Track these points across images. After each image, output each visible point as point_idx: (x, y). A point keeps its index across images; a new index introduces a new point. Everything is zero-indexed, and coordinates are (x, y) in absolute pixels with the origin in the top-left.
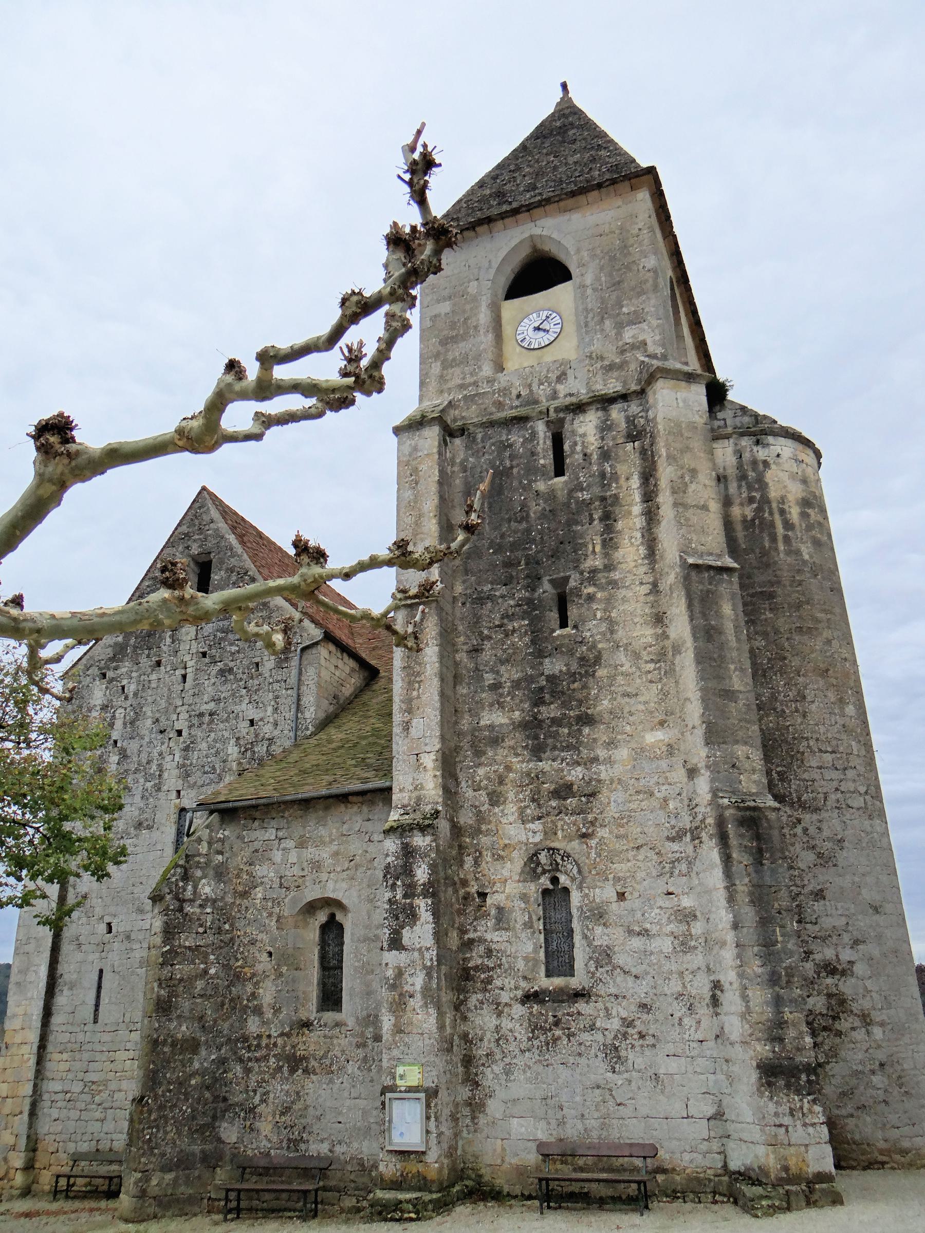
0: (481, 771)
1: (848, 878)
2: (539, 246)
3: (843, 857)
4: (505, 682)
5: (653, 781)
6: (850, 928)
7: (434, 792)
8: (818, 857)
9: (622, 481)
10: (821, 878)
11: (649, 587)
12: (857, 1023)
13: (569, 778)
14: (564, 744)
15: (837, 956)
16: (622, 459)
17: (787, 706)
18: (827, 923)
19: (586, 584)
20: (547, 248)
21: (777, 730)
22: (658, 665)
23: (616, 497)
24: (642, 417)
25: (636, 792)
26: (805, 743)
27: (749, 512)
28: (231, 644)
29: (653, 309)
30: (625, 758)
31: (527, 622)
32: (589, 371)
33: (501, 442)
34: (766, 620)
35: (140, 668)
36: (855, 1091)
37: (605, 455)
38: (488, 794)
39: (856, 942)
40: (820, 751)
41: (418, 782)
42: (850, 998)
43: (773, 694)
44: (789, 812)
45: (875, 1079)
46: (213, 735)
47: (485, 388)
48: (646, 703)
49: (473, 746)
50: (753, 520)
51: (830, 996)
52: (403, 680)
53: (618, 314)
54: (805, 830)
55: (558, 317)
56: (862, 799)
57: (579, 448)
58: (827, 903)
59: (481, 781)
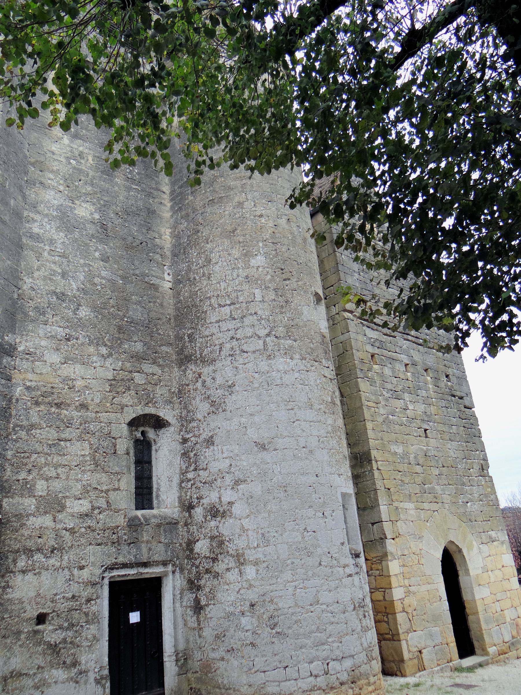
1: (236, 420)
3: (231, 401)
6: (233, 469)
8: (212, 406)
10: (213, 425)
12: (232, 564)
15: (220, 498)
18: (214, 467)
26: (208, 303)
36: (227, 634)
39: (237, 482)
40: (220, 306)
42: (227, 539)
44: (194, 370)
45: (244, 621)
51: (212, 538)
54: (204, 382)
56: (261, 342)
58: (216, 448)
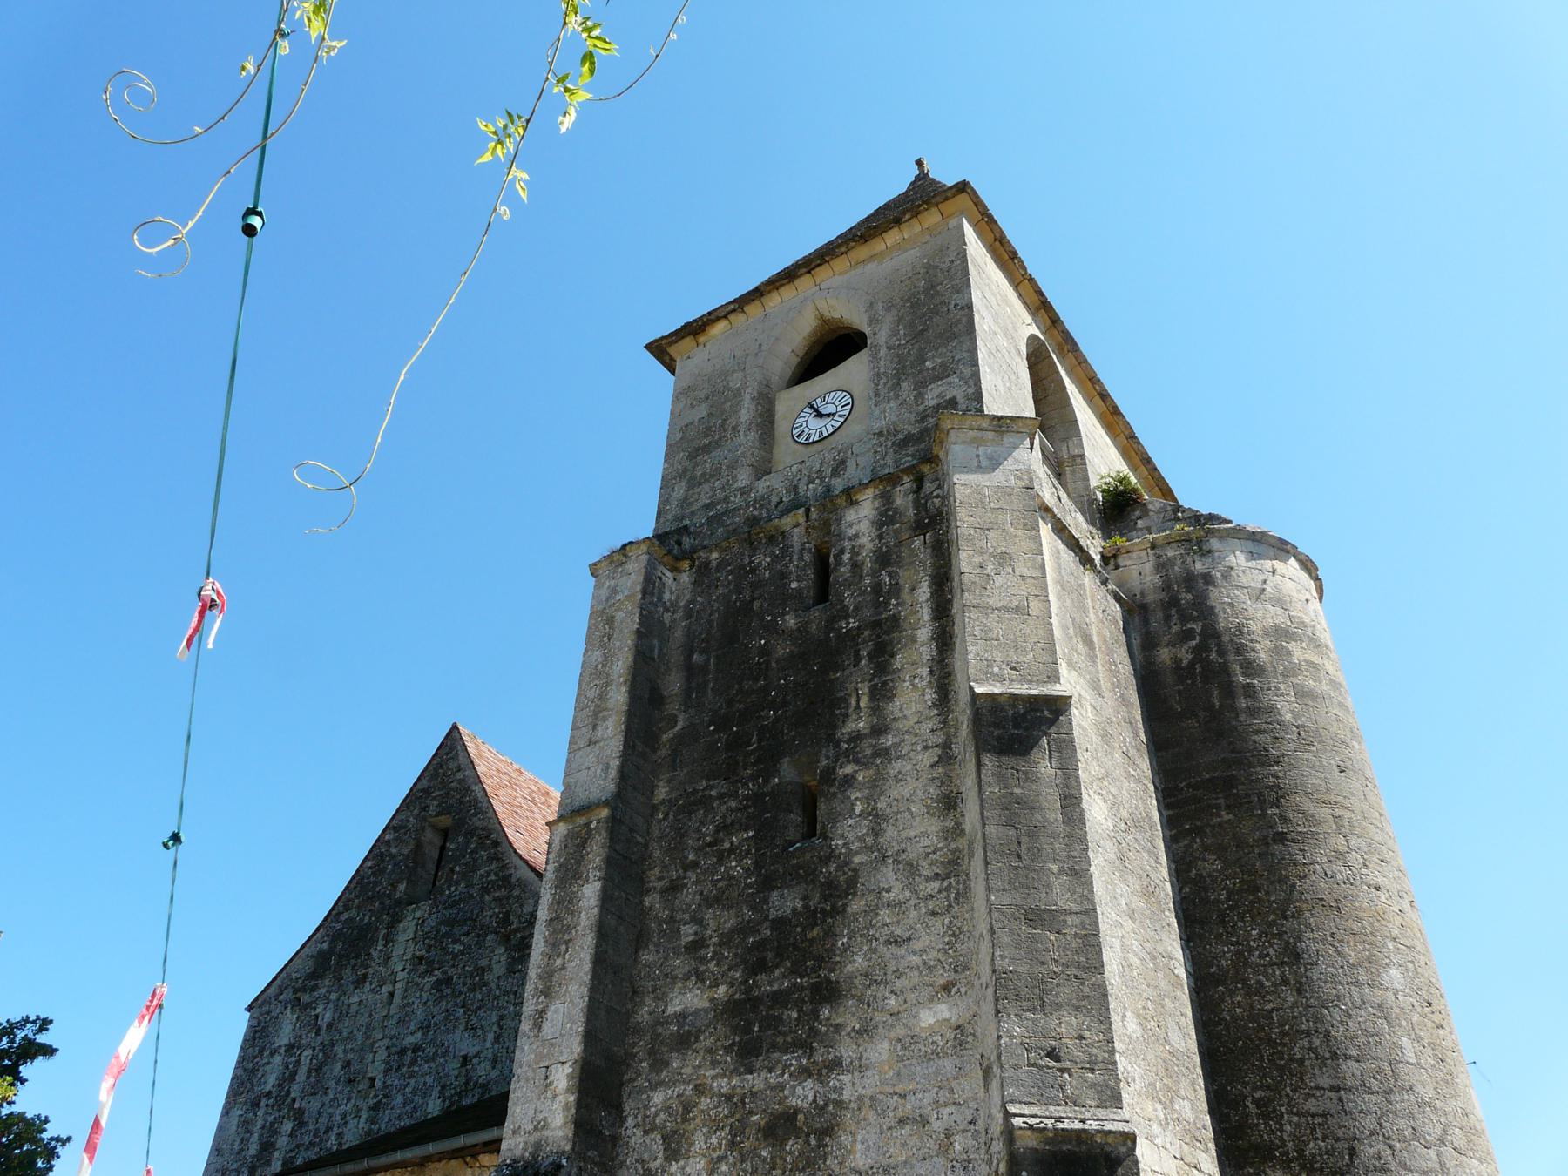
0: (658, 1098)
2: (827, 315)
4: (711, 937)
5: (929, 1098)
7: (561, 1134)
9: (905, 595)
11: (938, 751)
13: (793, 1101)
14: (789, 1039)
16: (907, 560)
17: (1266, 975)
19: (843, 760)
20: (836, 315)
21: (1252, 1019)
22: (945, 884)
23: (895, 619)
24: (937, 496)
25: (900, 1121)
27: (1185, 654)
28: (455, 942)
29: (965, 355)
30: (885, 1057)
31: (750, 834)
32: (876, 452)
33: (743, 567)
34: (1220, 825)
35: (341, 986)
37: (884, 559)
38: (664, 1138)
41: (541, 1116)
43: (1239, 953)
46: (412, 1081)
47: (737, 500)
48: (923, 951)
49: (652, 1053)
50: (1192, 664)
52: (546, 941)
53: (920, 372)
55: (849, 396)
57: (846, 556)
59: (656, 1115)
